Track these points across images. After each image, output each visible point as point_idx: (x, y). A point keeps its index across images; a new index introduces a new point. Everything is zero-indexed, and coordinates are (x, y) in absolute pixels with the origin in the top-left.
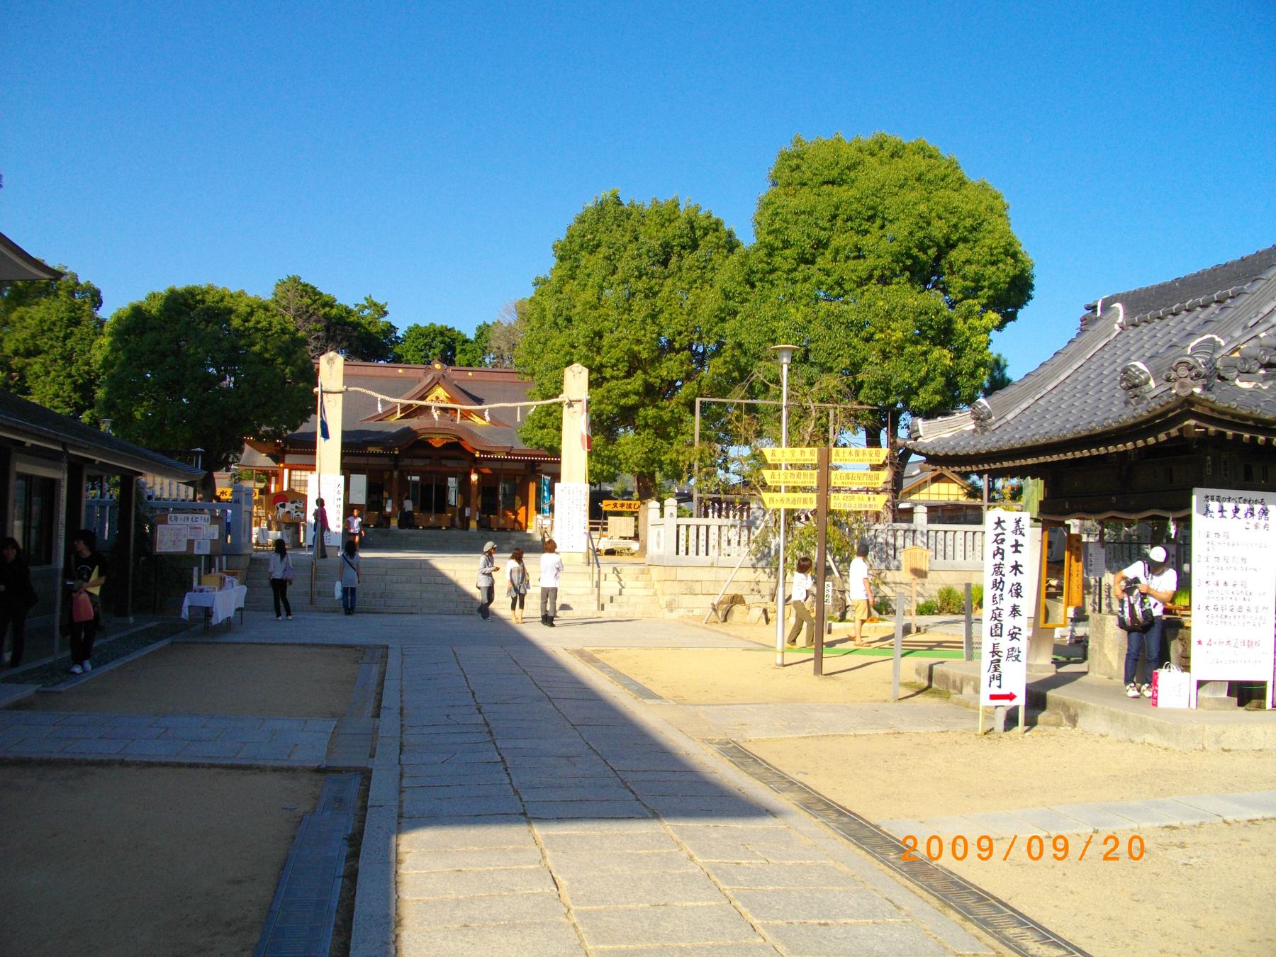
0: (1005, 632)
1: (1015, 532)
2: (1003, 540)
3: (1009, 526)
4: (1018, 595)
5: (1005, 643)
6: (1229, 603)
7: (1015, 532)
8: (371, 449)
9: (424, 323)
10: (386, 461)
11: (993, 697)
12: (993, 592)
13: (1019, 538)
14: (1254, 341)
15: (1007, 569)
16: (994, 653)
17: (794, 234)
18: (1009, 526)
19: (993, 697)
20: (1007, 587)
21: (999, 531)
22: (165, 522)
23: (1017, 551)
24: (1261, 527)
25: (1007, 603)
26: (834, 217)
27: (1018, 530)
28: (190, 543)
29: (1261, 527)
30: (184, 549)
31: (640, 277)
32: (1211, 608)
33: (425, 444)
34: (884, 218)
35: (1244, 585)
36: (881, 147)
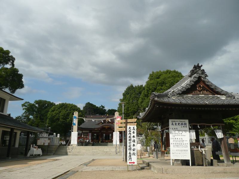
0: (132, 149)
1: (133, 130)
2: (131, 131)
3: (132, 128)
4: (134, 142)
5: (132, 152)
6: (178, 143)
7: (133, 130)
8: (96, 129)
9: (111, 109)
10: (98, 131)
11: (130, 163)
12: (129, 141)
13: (134, 131)
14: (178, 90)
15: (132, 137)
16: (130, 154)
17: (151, 87)
18: (132, 128)
19: (130, 163)
20: (132, 141)
21: (130, 129)
22: (39, 140)
23: (134, 133)
24: (185, 127)
25: (132, 143)
26: (157, 84)
27: (134, 129)
28: (44, 143)
29: (185, 127)
30: (43, 144)
31: (135, 98)
32: (174, 144)
33: (105, 128)
34: (165, 83)
35: (182, 139)
36: (168, 72)
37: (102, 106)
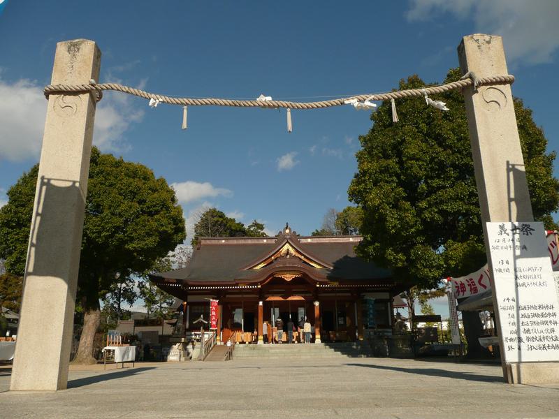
37: (256, 224)
